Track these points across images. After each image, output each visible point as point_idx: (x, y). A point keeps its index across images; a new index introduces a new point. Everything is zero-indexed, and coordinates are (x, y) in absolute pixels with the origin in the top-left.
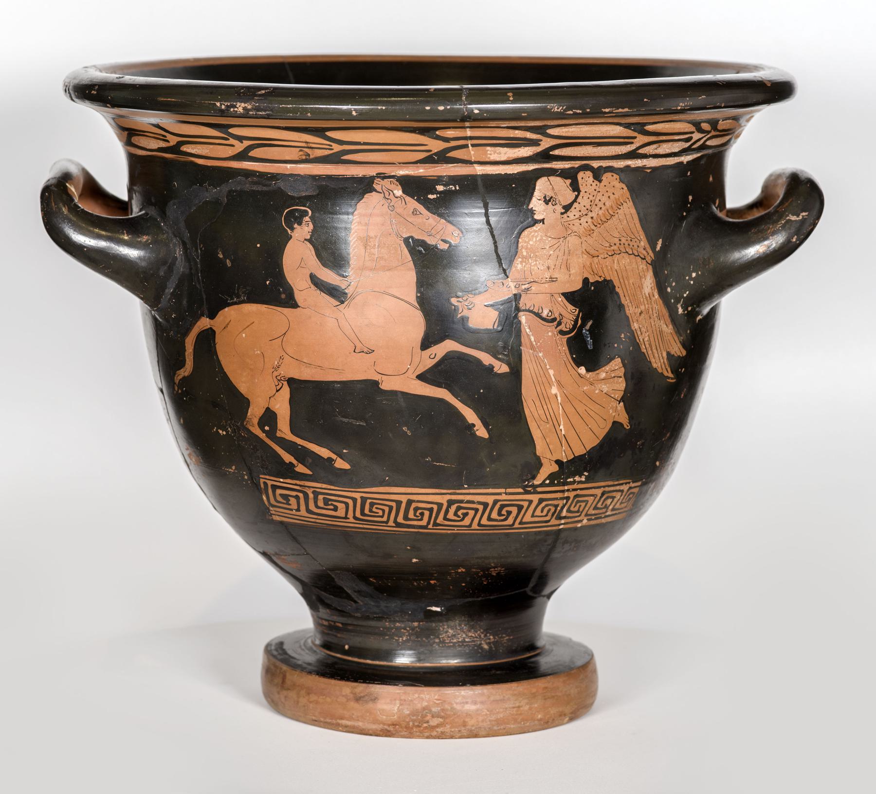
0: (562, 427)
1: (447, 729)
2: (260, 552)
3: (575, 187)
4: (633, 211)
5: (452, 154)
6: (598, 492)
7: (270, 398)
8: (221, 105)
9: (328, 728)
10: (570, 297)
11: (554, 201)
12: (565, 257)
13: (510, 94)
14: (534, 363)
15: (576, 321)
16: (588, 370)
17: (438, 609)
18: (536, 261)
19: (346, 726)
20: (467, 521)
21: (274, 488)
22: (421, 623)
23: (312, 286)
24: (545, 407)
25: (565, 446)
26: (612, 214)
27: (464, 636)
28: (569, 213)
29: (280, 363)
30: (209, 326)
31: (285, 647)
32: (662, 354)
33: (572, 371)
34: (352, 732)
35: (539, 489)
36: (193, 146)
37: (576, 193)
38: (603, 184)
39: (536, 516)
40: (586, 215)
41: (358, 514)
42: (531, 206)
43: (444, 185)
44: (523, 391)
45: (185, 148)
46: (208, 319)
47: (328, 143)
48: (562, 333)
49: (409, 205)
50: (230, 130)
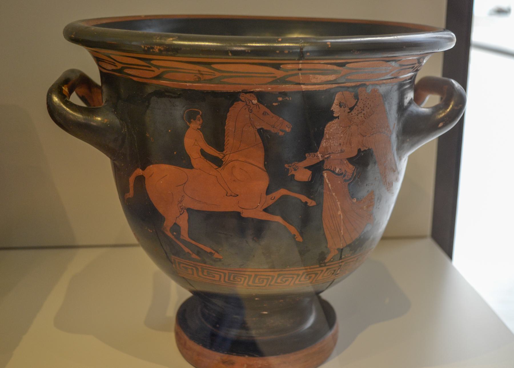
0: (342, 231)
5: (289, 79)
7: (176, 218)
10: (350, 160)
11: (344, 105)
15: (353, 174)
17: (266, 313)
18: (333, 141)
23: (202, 157)
24: (334, 222)
28: (352, 112)
29: (182, 200)
30: (142, 174)
36: (131, 70)
40: (361, 112)
42: (332, 109)
45: (126, 71)
46: (141, 170)
47: (212, 71)
48: (345, 181)
50: (152, 62)
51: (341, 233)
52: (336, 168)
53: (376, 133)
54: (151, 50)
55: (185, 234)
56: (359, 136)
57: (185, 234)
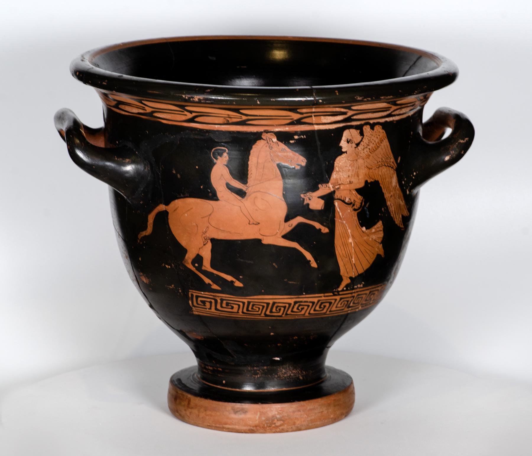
0: (353, 260)
1: (285, 427)
2: (178, 331)
3: (362, 134)
4: (388, 144)
5: (304, 120)
6: (368, 292)
7: (199, 249)
8: (185, 96)
9: (217, 430)
10: (359, 191)
12: (357, 171)
13: (336, 91)
14: (341, 227)
15: (361, 203)
16: (367, 229)
17: (278, 359)
19: (228, 429)
20: (303, 312)
21: (197, 297)
22: (268, 367)
24: (346, 249)
25: (354, 270)
26: (378, 145)
27: (291, 372)
30: (164, 209)
31: (183, 382)
32: (400, 216)
33: (359, 230)
34: (232, 432)
35: (341, 293)
36: (161, 114)
37: (362, 137)
38: (375, 131)
39: (339, 307)
40: (367, 147)
41: (245, 311)
43: (298, 136)
44: (336, 242)
48: (355, 210)
49: (280, 147)
51: (353, 261)
52: (345, 198)
53: (381, 166)
54: (191, 99)
55: (207, 265)
56: (366, 169)
57: (207, 265)
